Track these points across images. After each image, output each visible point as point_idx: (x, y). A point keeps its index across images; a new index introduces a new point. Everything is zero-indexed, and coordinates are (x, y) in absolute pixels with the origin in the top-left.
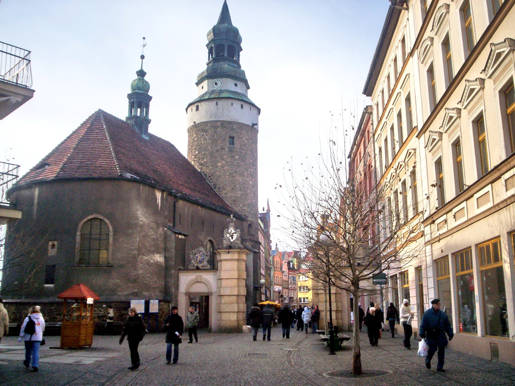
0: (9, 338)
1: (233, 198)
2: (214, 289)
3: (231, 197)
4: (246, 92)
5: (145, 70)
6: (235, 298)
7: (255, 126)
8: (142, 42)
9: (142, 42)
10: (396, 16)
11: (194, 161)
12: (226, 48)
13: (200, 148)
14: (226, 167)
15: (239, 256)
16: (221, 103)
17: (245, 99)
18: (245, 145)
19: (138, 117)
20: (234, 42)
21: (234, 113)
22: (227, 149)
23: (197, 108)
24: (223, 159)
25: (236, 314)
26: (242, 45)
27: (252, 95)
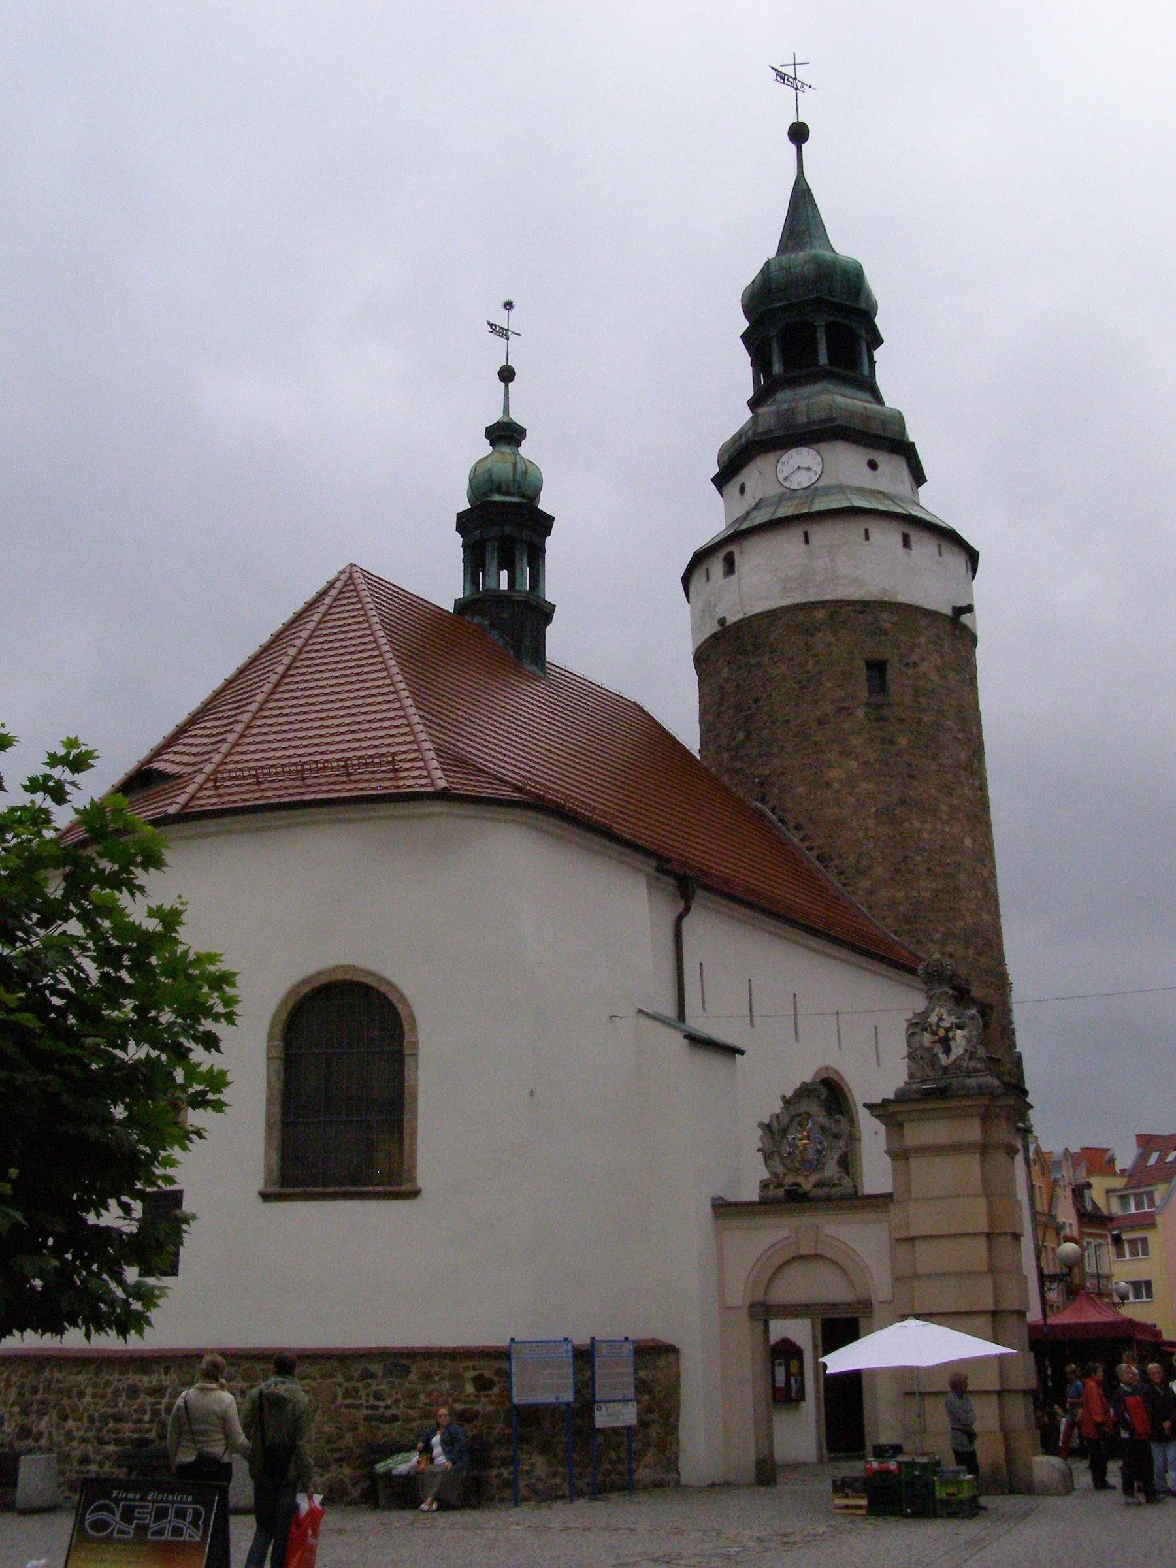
0: (456, 1517)
3: (892, 903)
4: (914, 492)
7: (965, 619)
9: (495, 354)
12: (821, 336)
14: (864, 785)
15: (984, 1130)
16: (821, 534)
21: (872, 568)
22: (860, 713)
23: (730, 566)
24: (846, 752)
26: (881, 321)
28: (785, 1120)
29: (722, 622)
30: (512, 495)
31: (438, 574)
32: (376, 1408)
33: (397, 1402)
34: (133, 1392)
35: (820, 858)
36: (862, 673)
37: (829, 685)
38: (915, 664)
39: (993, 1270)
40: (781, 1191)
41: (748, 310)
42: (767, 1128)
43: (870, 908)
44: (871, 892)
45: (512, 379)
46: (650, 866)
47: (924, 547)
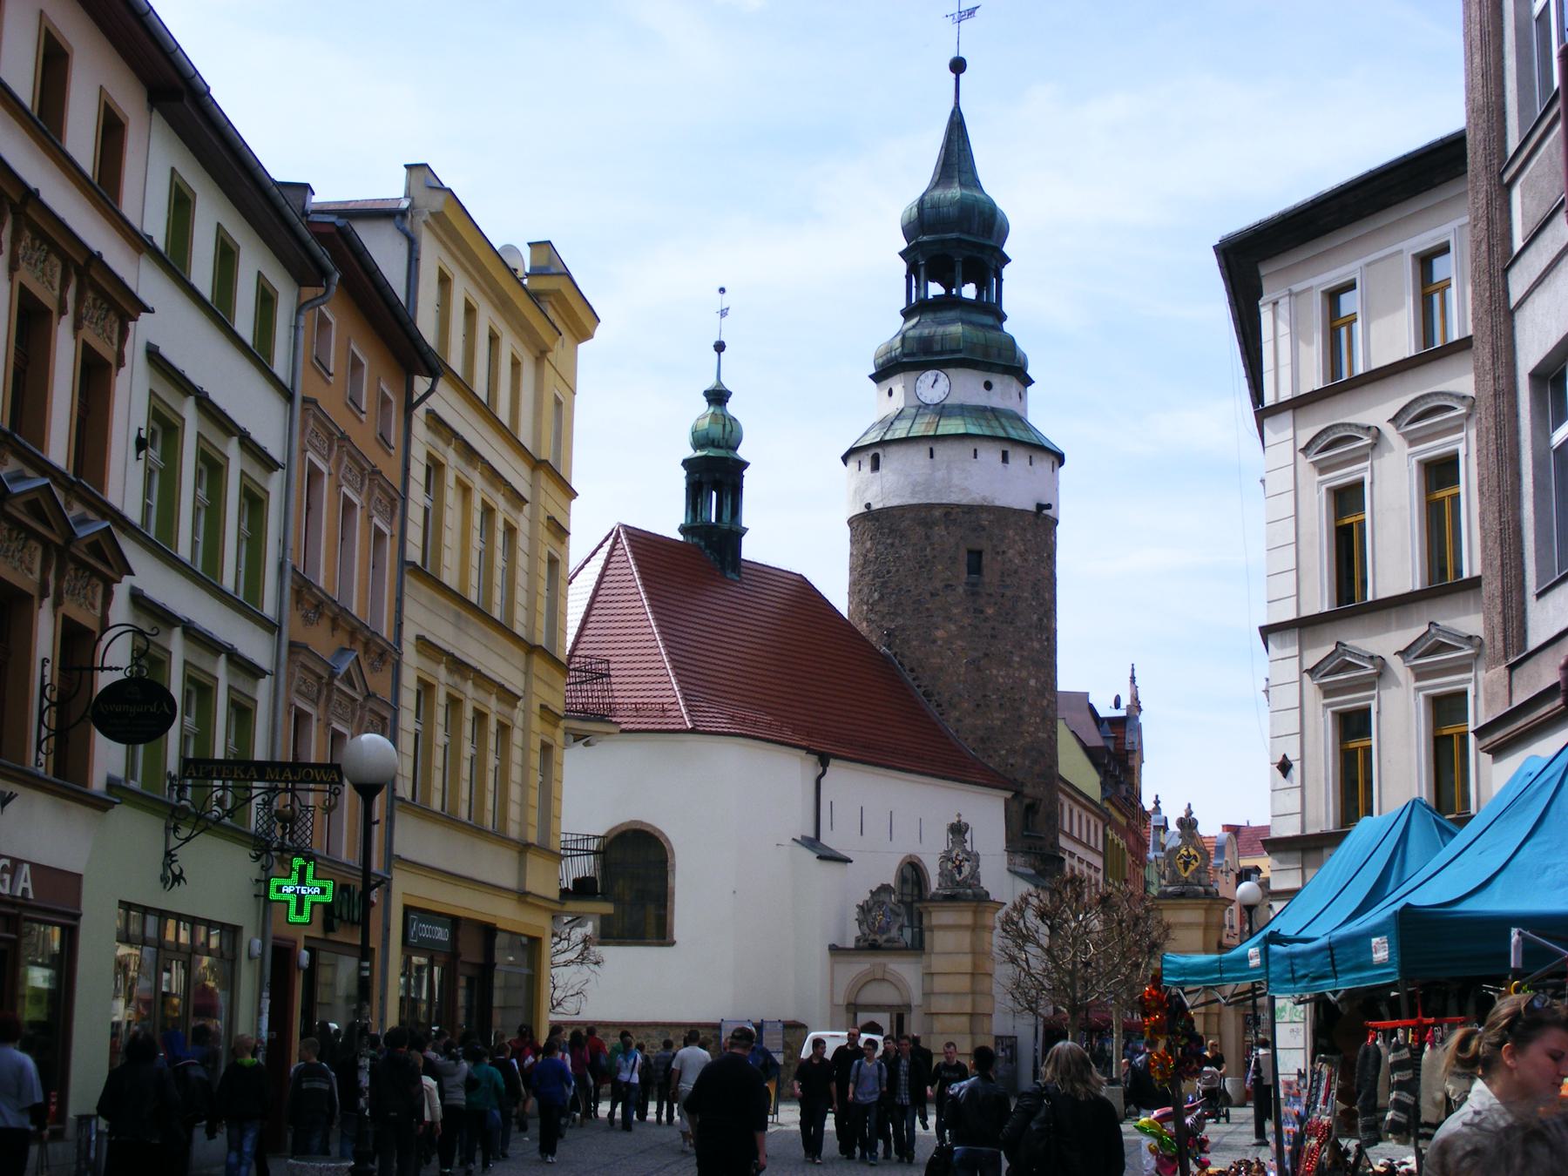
1: (981, 733)
2: (916, 998)
6: (965, 1020)
9: (719, 301)
11: (869, 621)
13: (884, 584)
14: (959, 643)
17: (1014, 434)
18: (1016, 572)
19: (713, 526)
20: (983, 247)
22: (960, 590)
24: (949, 619)
27: (1044, 411)
29: (868, 506)
31: (667, 516)
36: (963, 558)
39: (973, 993)
42: (861, 907)
44: (959, 720)
46: (803, 753)
47: (1019, 459)
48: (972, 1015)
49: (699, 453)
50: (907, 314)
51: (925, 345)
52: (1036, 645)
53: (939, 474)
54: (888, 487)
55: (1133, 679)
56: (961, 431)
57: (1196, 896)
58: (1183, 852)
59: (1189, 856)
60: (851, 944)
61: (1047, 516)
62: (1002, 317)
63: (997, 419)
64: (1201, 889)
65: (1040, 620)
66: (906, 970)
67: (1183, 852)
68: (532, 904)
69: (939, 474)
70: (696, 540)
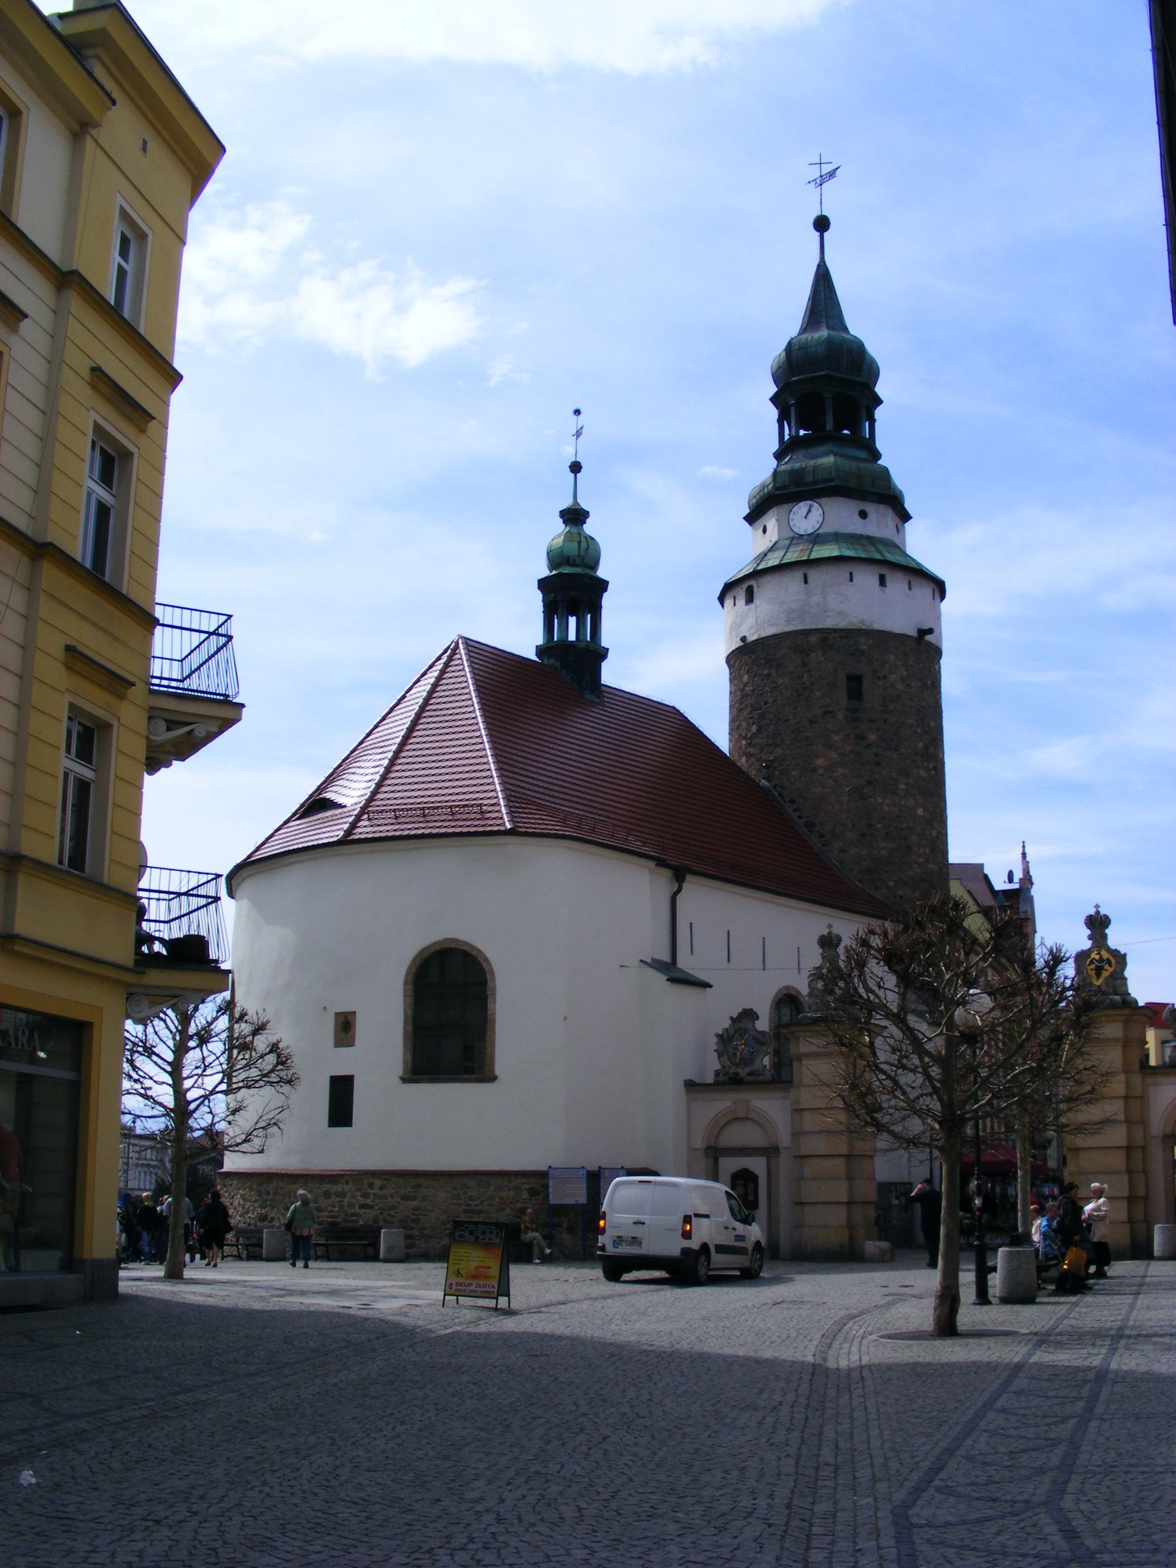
4: (899, 530)
5: (584, 505)
6: (840, 1163)
7: (928, 638)
8: (572, 423)
9: (572, 423)
10: (554, 827)
11: (748, 755)
13: (762, 716)
14: (841, 770)
17: (890, 557)
21: (861, 603)
22: (841, 716)
25: (843, 1210)
27: (921, 543)
28: (731, 1032)
30: (578, 566)
31: (521, 632)
32: (469, 1205)
33: (482, 1202)
34: (327, 1195)
35: (807, 825)
37: (818, 694)
38: (885, 677)
40: (726, 1078)
41: (776, 378)
43: (841, 862)
44: (842, 851)
45: (579, 471)
46: (652, 864)
47: (897, 584)
48: (849, 1157)
49: (554, 572)
50: (778, 456)
51: (797, 476)
52: (923, 773)
53: (814, 600)
54: (761, 618)
55: (1024, 855)
56: (835, 553)
57: (1113, 1006)
58: (1094, 955)
59: (1101, 960)
60: (710, 1079)
61: (929, 644)
62: (877, 455)
63: (873, 544)
64: (1117, 998)
65: (926, 748)
66: (772, 1108)
67: (1094, 955)
68: (19, 955)
69: (814, 600)
70: (552, 661)
